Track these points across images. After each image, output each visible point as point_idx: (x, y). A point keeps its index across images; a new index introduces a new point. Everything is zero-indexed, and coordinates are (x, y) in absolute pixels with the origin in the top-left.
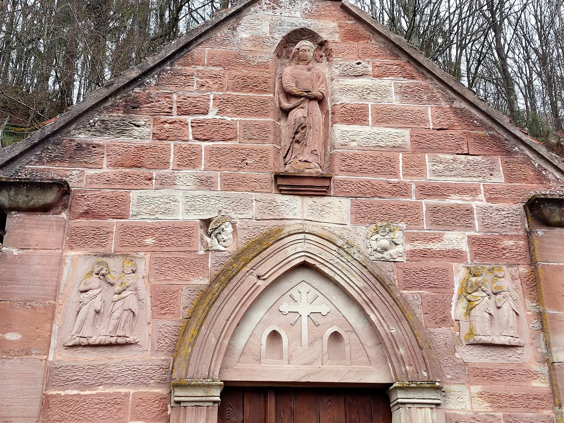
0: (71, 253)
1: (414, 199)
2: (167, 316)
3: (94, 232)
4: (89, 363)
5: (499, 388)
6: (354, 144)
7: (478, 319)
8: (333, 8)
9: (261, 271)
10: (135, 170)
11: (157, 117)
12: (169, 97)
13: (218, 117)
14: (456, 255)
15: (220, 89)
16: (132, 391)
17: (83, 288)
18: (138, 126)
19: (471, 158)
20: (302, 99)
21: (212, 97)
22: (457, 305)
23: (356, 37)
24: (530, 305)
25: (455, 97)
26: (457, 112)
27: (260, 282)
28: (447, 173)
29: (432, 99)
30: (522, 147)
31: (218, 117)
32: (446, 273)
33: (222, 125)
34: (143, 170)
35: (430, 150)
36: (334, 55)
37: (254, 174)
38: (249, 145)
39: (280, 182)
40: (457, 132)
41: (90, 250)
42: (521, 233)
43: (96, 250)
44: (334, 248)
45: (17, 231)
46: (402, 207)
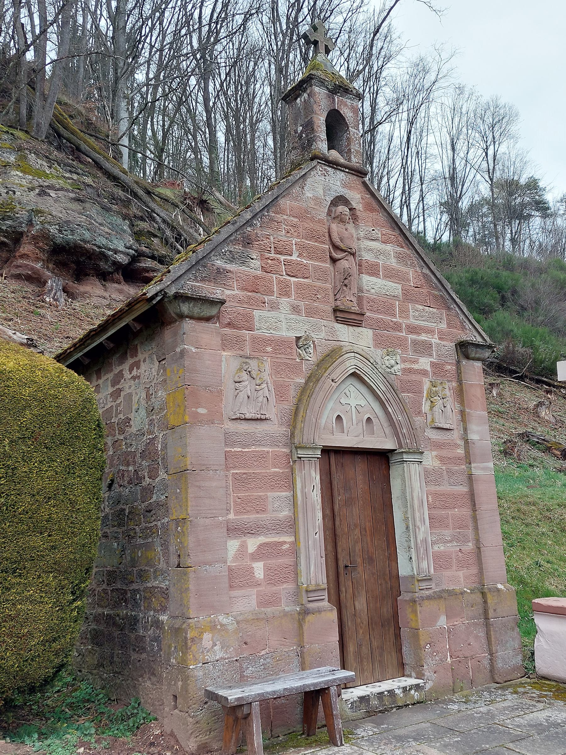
0: (225, 353)
1: (404, 334)
2: (284, 402)
3: (236, 339)
4: (245, 431)
5: (445, 453)
6: (373, 291)
7: (437, 413)
8: (358, 183)
9: (333, 376)
10: (254, 294)
11: (262, 253)
12: (269, 238)
13: (299, 259)
14: (424, 373)
15: (298, 237)
16: (271, 450)
17: (237, 379)
18: (252, 259)
19: (431, 309)
20: (346, 253)
21: (294, 242)
22: (425, 404)
23: (372, 210)
24: (457, 405)
25: (424, 265)
26: (425, 275)
27: (333, 384)
28: (420, 319)
29: (413, 266)
30: (455, 306)
31: (299, 259)
32: (420, 383)
33: (301, 266)
34: (259, 295)
35: (412, 301)
36: (360, 221)
37: (321, 306)
38: (318, 284)
39: (339, 314)
40: (425, 291)
41: (235, 352)
42: (454, 361)
43: (238, 352)
44: (370, 364)
45: (191, 334)
46: (399, 338)
